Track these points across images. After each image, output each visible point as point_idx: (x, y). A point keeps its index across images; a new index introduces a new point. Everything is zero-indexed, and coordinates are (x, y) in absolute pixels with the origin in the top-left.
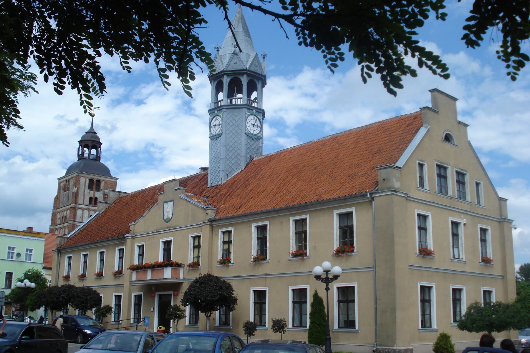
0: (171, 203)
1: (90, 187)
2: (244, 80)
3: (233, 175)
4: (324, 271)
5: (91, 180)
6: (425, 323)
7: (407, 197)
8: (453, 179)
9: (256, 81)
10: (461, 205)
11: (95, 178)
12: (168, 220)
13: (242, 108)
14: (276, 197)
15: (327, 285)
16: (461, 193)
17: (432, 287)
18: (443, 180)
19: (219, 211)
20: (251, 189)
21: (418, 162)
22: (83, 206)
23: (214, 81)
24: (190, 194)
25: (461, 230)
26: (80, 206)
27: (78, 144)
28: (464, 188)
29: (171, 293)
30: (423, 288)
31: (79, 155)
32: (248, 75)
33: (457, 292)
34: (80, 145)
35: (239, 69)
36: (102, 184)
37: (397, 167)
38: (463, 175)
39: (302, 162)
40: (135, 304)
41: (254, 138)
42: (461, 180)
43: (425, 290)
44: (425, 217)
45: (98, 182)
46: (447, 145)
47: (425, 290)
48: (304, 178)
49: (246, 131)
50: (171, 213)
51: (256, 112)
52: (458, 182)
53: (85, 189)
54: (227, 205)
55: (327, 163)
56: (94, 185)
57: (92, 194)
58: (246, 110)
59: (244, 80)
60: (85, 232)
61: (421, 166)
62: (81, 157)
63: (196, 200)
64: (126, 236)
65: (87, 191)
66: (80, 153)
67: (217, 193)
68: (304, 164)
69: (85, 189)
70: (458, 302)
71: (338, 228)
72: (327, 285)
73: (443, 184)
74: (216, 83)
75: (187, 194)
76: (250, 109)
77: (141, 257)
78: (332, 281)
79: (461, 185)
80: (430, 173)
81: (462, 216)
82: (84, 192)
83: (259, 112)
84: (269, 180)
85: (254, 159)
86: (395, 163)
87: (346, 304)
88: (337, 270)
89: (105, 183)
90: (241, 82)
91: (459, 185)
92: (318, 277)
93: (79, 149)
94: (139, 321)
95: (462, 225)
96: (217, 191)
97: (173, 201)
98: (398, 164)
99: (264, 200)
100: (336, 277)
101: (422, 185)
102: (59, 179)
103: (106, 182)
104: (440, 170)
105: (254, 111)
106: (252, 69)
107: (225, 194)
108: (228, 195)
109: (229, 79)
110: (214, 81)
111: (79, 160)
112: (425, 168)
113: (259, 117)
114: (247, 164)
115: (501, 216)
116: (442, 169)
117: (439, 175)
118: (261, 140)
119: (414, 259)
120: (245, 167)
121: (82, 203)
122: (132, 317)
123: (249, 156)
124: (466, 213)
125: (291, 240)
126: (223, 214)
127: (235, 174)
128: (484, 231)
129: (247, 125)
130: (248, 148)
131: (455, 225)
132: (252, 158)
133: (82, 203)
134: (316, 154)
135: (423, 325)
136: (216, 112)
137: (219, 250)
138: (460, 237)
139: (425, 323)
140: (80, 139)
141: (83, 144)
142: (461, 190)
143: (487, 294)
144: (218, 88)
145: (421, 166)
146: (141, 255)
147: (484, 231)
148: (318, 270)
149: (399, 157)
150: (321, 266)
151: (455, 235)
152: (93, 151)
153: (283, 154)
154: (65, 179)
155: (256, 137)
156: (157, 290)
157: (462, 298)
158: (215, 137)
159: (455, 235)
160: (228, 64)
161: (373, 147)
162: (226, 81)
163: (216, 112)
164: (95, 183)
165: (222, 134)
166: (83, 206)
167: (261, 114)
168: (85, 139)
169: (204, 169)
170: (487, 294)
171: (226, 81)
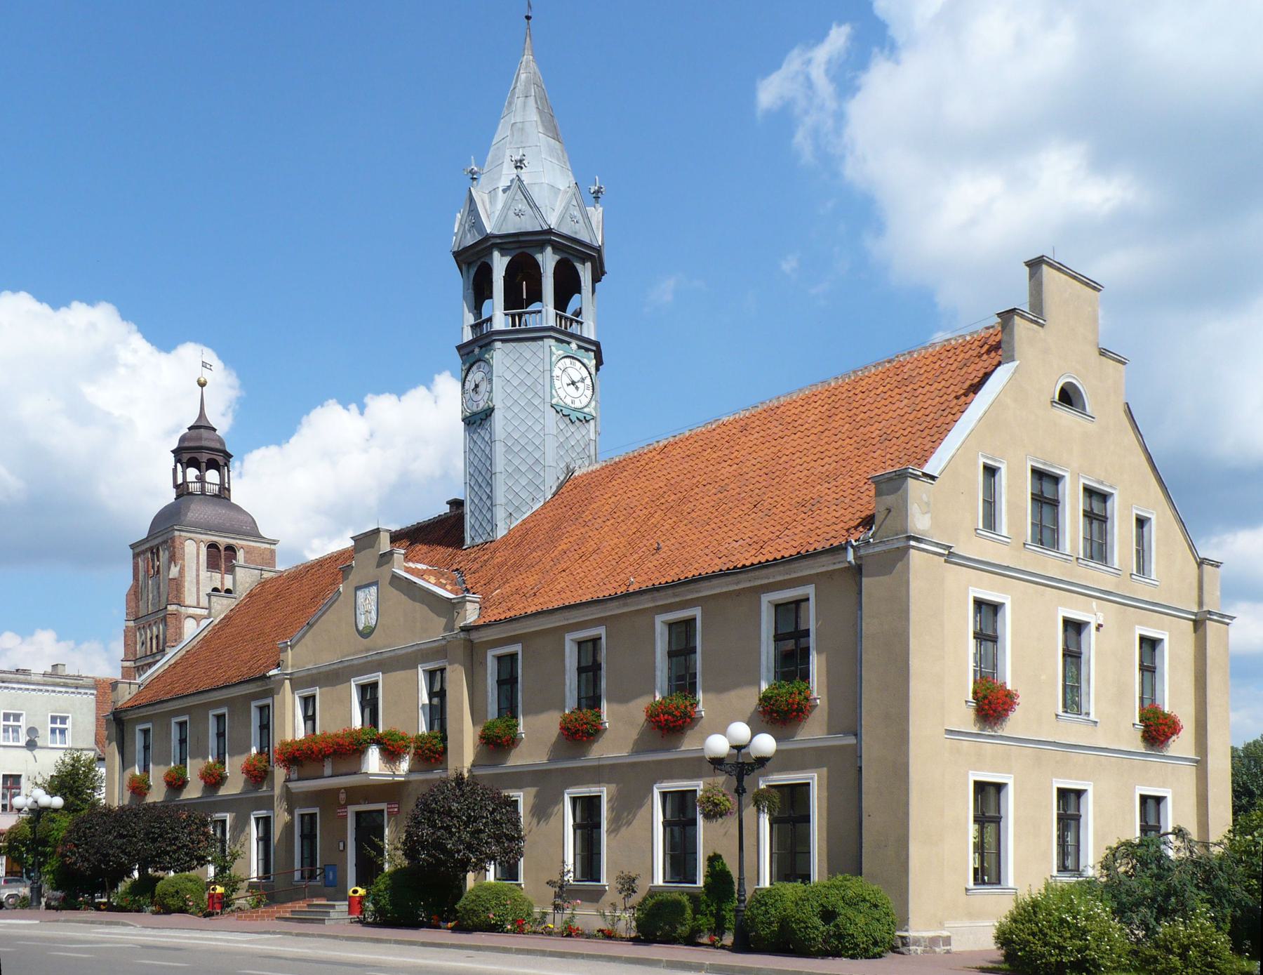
0: (373, 590)
1: (213, 564)
2: (548, 261)
3: (525, 516)
4: (733, 747)
5: (212, 546)
6: (988, 871)
7: (950, 556)
8: (1074, 508)
9: (579, 266)
10: (1096, 575)
11: (223, 541)
12: (366, 633)
13: (541, 338)
14: (623, 566)
15: (740, 780)
16: (1095, 545)
17: (1005, 784)
18: (1046, 509)
19: (487, 604)
20: (564, 547)
21: (981, 461)
22: (198, 611)
23: (469, 265)
24: (420, 566)
25: (1091, 642)
26: (191, 611)
27: (172, 457)
28: (1103, 533)
29: (383, 806)
30: (980, 787)
31: (176, 486)
32: (557, 248)
33: (1069, 798)
34: (178, 461)
35: (530, 229)
36: (241, 555)
37: (925, 475)
38: (1104, 497)
39: (689, 475)
40: (303, 836)
41: (574, 419)
42: (1096, 511)
43: (987, 793)
44: (995, 608)
45: (231, 549)
46: (1065, 415)
47: (987, 793)
48: (693, 515)
49: (554, 401)
50: (374, 615)
51: (580, 347)
52: (1089, 515)
53: (198, 570)
54: (507, 589)
55: (751, 474)
56: (220, 558)
57: (216, 579)
58: (552, 342)
59: (548, 261)
60: (179, 669)
61: (990, 471)
62: (182, 490)
63: (433, 580)
64: (271, 673)
65: (204, 574)
66: (180, 481)
67: (486, 561)
68: (695, 481)
69: (198, 570)
70: (1073, 823)
71: (772, 639)
72: (740, 780)
73: (1047, 522)
74: (473, 272)
75: (411, 565)
76: (562, 341)
77: (309, 723)
78: (753, 770)
79: (1096, 524)
80: (1015, 493)
81: (1094, 603)
82: (198, 576)
83: (587, 350)
84: (608, 523)
85: (576, 474)
86: (920, 466)
87: (789, 826)
88: (766, 744)
89: (246, 553)
90: (536, 266)
91: (1091, 523)
92: (717, 762)
93: (175, 470)
94: (312, 876)
95: (1093, 627)
96: (486, 557)
97: (376, 583)
98: (928, 469)
99: (594, 573)
100: (762, 761)
101: (990, 521)
102: (133, 546)
103: (249, 552)
104: (1091, 523)
105: (574, 346)
106: (565, 230)
107: (504, 563)
108: (512, 565)
109: (507, 260)
110: (469, 265)
111: (178, 497)
112: (1003, 478)
113: (585, 361)
114: (560, 487)
115: (1201, 604)
116: (1044, 479)
117: (1038, 499)
118: (592, 422)
119: (964, 717)
120: (554, 495)
121: (195, 604)
122: (297, 865)
123: (562, 465)
124: (1105, 596)
125: (658, 673)
126: (496, 611)
127: (528, 514)
128: (1150, 645)
129: (557, 384)
130: (561, 445)
131: (1074, 628)
132: (570, 471)
133: (195, 604)
134: (727, 452)
135: (981, 876)
136: (477, 350)
137: (490, 700)
138: (1084, 658)
139: (988, 871)
140: (175, 445)
141: (186, 457)
142: (1095, 539)
143: (1151, 804)
144: (480, 290)
145: (990, 471)
146: (309, 718)
147: (1150, 645)
148: (718, 745)
149: (932, 451)
150: (724, 733)
151: (1072, 656)
152: (212, 476)
153: (646, 457)
154: (148, 545)
155: (581, 416)
156: (350, 801)
157: (1082, 812)
158: (478, 417)
159: (1072, 656)
160: (504, 218)
161: (869, 427)
162: (500, 264)
163: (477, 350)
164: (223, 553)
165: (492, 410)
166: (198, 611)
167: (592, 354)
168: (186, 444)
169: (457, 504)
170: (1151, 804)
171: (500, 264)
